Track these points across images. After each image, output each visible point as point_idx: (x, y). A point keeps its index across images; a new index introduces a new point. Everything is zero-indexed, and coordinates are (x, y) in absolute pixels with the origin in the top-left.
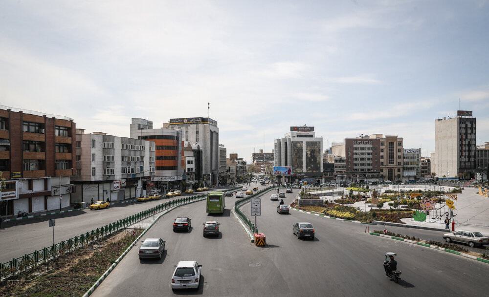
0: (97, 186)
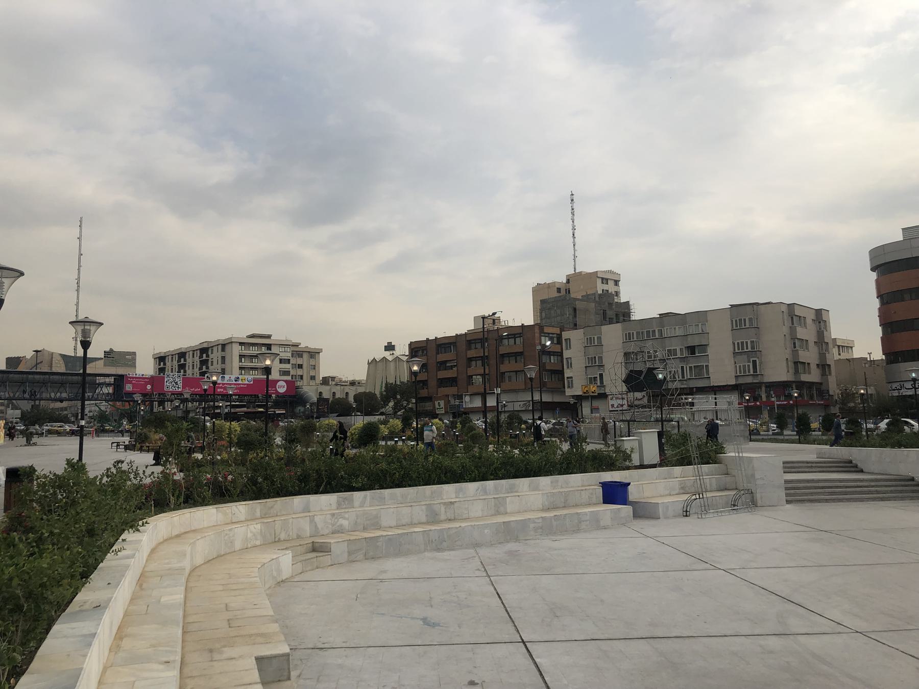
0: (508, 358)
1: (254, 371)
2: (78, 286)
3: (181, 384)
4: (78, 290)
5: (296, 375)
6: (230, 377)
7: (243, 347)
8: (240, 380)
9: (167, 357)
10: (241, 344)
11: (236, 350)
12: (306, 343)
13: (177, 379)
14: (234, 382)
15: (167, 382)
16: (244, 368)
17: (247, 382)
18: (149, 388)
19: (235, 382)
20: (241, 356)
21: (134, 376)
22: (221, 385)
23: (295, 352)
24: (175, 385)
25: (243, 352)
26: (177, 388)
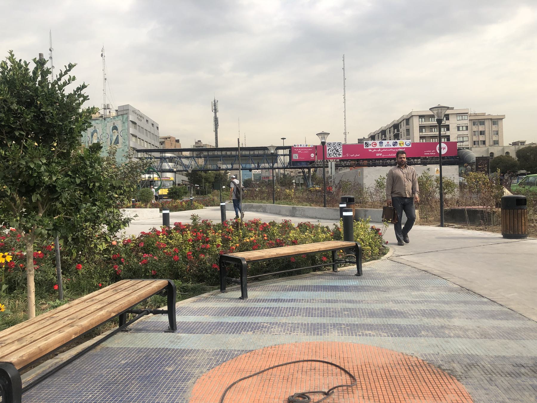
1: (434, 140)
2: (345, 100)
3: (342, 151)
4: (344, 102)
5: (478, 141)
6: (388, 143)
7: (423, 119)
8: (398, 145)
9: (377, 135)
10: (421, 117)
11: (416, 123)
12: (493, 111)
13: (337, 147)
14: (392, 147)
15: (328, 150)
16: (425, 137)
17: (405, 146)
18: (312, 156)
19: (393, 147)
20: (421, 128)
21: (299, 147)
22: (380, 150)
23: (477, 121)
24: (336, 152)
25: (423, 123)
26: (338, 155)
